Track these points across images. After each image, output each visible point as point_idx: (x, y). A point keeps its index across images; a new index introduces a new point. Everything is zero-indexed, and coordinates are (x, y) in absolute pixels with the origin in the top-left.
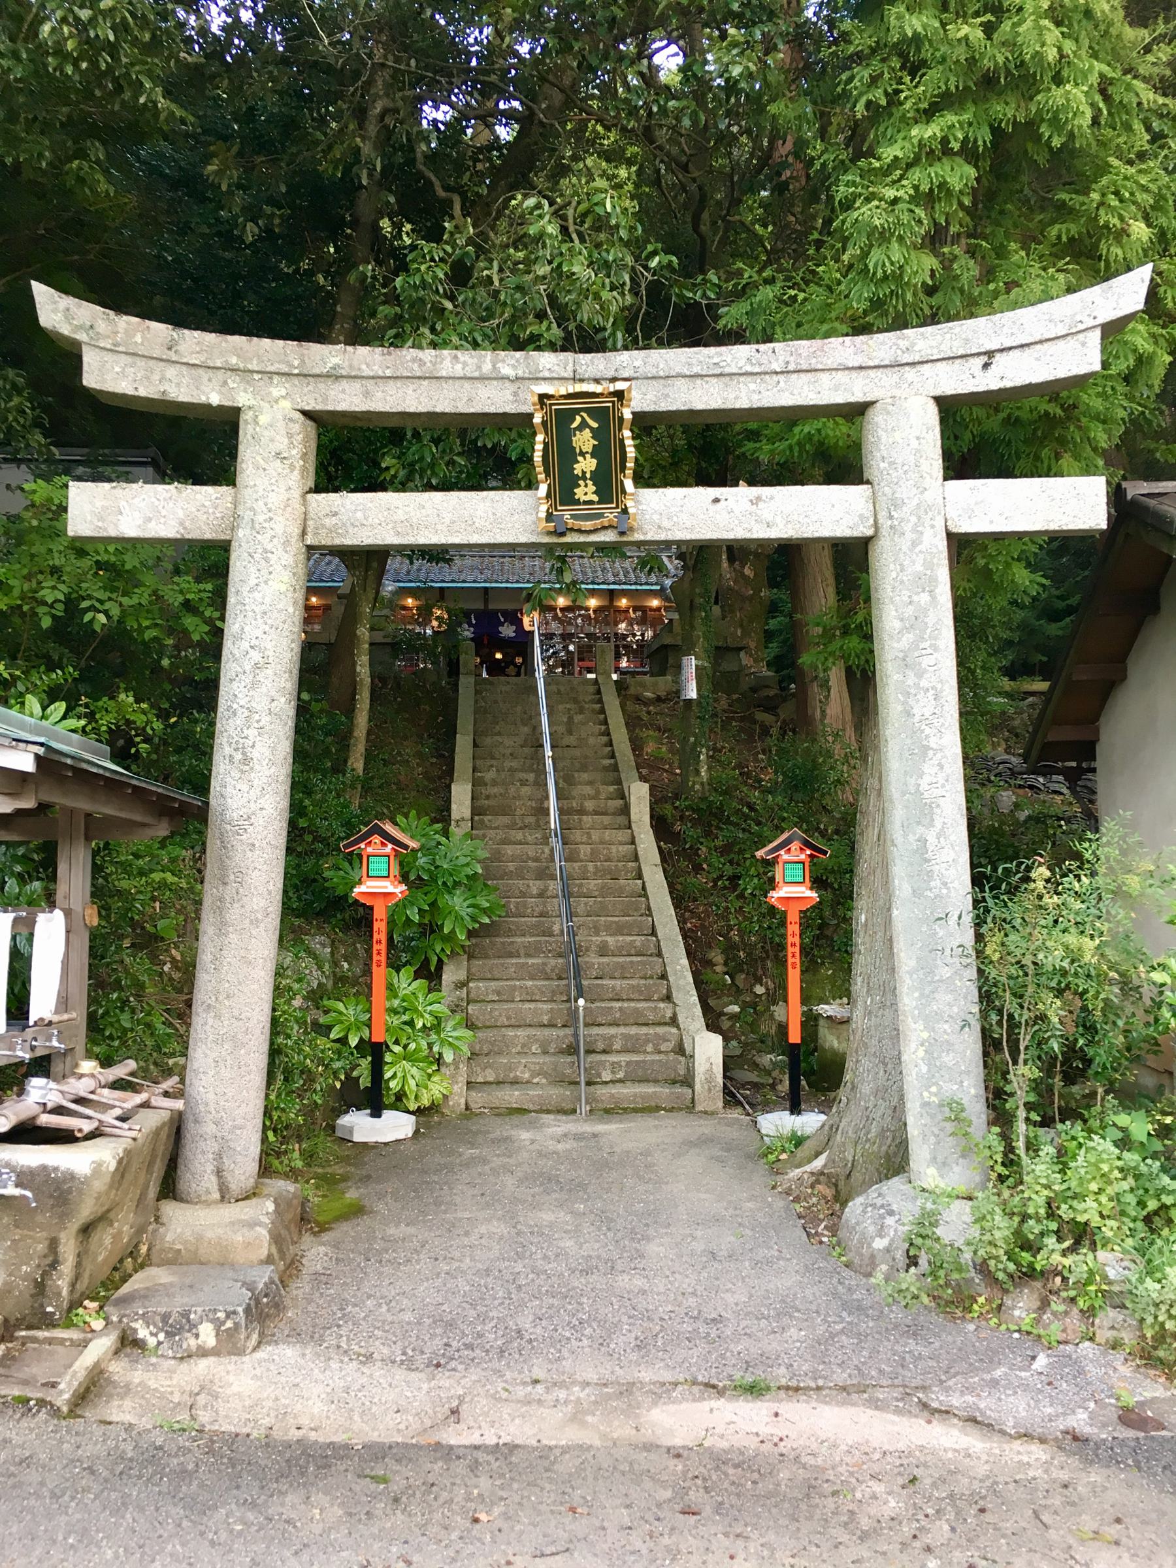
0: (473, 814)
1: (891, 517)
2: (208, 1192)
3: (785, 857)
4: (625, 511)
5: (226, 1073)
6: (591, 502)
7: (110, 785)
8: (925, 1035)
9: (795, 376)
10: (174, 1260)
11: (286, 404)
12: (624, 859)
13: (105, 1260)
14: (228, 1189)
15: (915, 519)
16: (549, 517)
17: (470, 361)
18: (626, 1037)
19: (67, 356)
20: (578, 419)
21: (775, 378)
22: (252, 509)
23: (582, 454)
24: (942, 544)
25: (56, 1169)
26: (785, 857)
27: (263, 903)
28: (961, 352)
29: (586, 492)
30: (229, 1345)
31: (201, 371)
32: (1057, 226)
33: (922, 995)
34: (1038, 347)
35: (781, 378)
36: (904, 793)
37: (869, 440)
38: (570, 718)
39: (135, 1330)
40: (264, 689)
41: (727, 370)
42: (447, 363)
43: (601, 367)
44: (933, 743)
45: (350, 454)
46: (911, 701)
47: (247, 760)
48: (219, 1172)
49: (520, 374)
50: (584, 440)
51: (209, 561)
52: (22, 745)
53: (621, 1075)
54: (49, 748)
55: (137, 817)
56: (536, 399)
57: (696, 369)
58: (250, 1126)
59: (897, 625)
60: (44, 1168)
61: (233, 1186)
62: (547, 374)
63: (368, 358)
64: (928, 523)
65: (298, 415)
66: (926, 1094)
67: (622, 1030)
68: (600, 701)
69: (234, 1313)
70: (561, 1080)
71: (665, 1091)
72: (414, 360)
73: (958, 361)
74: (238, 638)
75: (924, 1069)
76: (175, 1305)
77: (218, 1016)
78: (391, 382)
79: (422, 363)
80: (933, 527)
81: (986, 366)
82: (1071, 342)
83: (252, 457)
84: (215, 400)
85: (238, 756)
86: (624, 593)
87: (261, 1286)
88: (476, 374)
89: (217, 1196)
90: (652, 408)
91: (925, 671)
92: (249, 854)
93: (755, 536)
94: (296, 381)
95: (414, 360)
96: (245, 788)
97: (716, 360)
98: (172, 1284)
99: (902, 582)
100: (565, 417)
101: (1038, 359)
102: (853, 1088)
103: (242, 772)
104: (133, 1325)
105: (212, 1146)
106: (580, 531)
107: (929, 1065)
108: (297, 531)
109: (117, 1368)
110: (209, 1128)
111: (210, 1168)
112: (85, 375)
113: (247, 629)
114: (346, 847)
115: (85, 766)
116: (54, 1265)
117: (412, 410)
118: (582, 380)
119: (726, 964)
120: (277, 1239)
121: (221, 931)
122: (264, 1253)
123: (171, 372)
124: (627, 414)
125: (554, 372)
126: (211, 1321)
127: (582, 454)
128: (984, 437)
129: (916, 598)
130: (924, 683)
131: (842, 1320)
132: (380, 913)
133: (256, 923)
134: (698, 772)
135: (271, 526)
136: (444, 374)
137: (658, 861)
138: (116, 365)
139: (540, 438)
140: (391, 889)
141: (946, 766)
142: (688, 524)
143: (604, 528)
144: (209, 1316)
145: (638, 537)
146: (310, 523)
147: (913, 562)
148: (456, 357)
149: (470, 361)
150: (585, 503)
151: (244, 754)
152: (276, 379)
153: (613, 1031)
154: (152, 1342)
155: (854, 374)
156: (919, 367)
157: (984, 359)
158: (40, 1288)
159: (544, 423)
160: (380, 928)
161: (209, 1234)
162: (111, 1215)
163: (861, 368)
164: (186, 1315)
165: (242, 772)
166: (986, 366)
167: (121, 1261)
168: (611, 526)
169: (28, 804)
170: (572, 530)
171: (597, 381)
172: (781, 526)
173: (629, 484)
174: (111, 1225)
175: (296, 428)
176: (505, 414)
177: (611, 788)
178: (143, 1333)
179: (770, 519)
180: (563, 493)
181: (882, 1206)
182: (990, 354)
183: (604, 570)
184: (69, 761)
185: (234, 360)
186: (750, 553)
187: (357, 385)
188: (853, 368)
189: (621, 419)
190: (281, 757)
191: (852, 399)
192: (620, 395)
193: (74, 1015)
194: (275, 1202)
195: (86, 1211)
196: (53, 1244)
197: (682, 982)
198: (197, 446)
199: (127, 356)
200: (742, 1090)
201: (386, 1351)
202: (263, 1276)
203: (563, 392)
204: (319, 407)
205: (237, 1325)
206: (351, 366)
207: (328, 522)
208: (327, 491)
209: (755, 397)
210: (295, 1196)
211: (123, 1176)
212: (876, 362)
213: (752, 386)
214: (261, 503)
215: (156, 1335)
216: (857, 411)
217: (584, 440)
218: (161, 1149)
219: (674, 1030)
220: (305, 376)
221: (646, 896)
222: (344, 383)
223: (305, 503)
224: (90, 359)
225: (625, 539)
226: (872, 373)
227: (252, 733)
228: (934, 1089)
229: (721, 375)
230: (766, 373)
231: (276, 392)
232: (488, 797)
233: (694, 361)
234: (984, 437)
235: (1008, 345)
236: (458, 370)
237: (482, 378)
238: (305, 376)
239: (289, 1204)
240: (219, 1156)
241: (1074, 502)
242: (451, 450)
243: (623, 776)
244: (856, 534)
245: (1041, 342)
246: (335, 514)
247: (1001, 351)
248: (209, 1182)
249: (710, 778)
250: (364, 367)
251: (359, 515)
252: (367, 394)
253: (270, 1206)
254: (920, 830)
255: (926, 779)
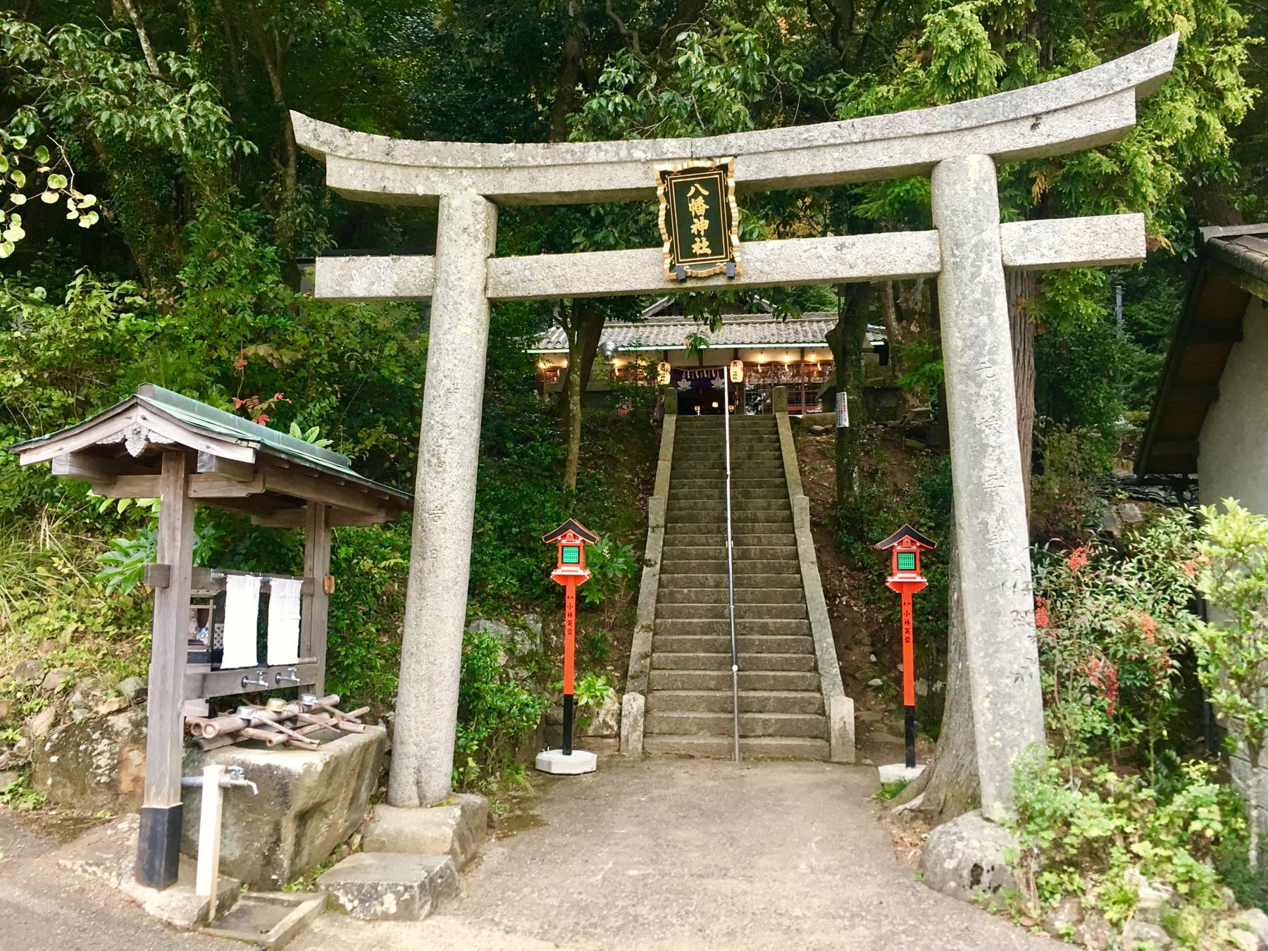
0: (666, 522)
1: (954, 256)
2: (410, 798)
3: (899, 548)
4: (733, 260)
5: (424, 706)
6: (706, 255)
7: (350, 485)
8: (990, 688)
9: (870, 145)
10: (381, 847)
11: (473, 192)
12: (787, 557)
13: (322, 844)
14: (425, 797)
15: (978, 253)
16: (672, 267)
17: (610, 149)
18: (779, 700)
19: (312, 165)
20: (693, 189)
21: (855, 147)
22: (446, 272)
23: (697, 217)
24: (1000, 277)
25: (277, 768)
26: (899, 548)
27: (452, 574)
28: (1012, 116)
29: (702, 246)
30: (406, 913)
31: (410, 170)
32: (1113, 14)
33: (987, 655)
34: (1080, 108)
35: (860, 147)
36: (968, 484)
37: (936, 192)
38: (751, 447)
39: (338, 897)
40: (454, 409)
41: (815, 143)
42: (593, 152)
43: (713, 147)
44: (992, 441)
45: (528, 225)
46: (973, 407)
47: (441, 463)
48: (418, 783)
49: (649, 157)
50: (698, 206)
51: (416, 313)
52: (245, 443)
53: (771, 731)
54: (264, 445)
55: (359, 508)
56: (658, 176)
57: (789, 145)
58: (442, 748)
59: (960, 343)
60: (269, 767)
61: (429, 795)
62: (670, 156)
63: (533, 152)
64: (985, 258)
65: (483, 200)
66: (991, 739)
67: (775, 694)
68: (777, 433)
69: (411, 887)
70: (722, 730)
71: (807, 742)
72: (567, 151)
73: (1009, 124)
74: (436, 370)
75: (990, 717)
76: (367, 879)
77: (418, 662)
78: (551, 169)
79: (573, 152)
80: (989, 261)
81: (1034, 126)
82: (1109, 102)
83: (446, 232)
84: (421, 190)
85: (434, 461)
86: (813, 350)
87: (437, 869)
88: (615, 159)
89: (417, 802)
90: (754, 178)
91: (984, 382)
92: (442, 536)
93: (840, 276)
94: (480, 173)
95: (567, 151)
96: (439, 484)
97: (805, 136)
98: (371, 866)
99: (964, 308)
100: (682, 189)
101: (1080, 118)
102: (947, 738)
103: (437, 472)
104: (336, 893)
105: (413, 763)
106: (697, 278)
107: (993, 714)
108: (481, 287)
109: (318, 925)
110: (411, 749)
111: (412, 779)
112: (328, 178)
113: (442, 363)
114: (547, 539)
115: (298, 461)
116: (277, 842)
117: (567, 190)
118: (698, 159)
119: (873, 645)
120: (461, 837)
121: (421, 597)
122: (447, 847)
123: (389, 172)
124: (731, 183)
125: (680, 151)
126: (394, 893)
127: (697, 217)
128: (1041, 184)
129: (975, 321)
130: (983, 392)
131: (905, 922)
132: (571, 592)
133: (447, 589)
134: (851, 488)
135: (463, 280)
136: (590, 160)
137: (815, 559)
138: (351, 168)
139: (663, 206)
140: (581, 573)
141: (1004, 460)
142: (785, 269)
143: (716, 274)
144: (392, 888)
145: (744, 280)
146: (491, 280)
147: (973, 291)
148: (599, 147)
149: (610, 149)
150: (701, 255)
151: (439, 458)
152: (465, 172)
153: (766, 694)
154: (349, 906)
155: (921, 140)
156: (976, 131)
157: (1032, 121)
158: (269, 861)
159: (666, 194)
160: (571, 602)
161: (407, 830)
162: (326, 808)
163: (927, 134)
164: (375, 887)
165: (437, 472)
166: (1034, 126)
167: (338, 846)
168: (722, 273)
169: (258, 489)
170: (691, 277)
171: (710, 158)
172: (861, 267)
173: (735, 239)
174: (326, 817)
175: (480, 208)
176: (638, 189)
177: (781, 501)
178: (343, 900)
179: (852, 261)
180: (684, 248)
181: (955, 833)
182: (1037, 116)
183: (796, 332)
184: (283, 456)
185: (434, 160)
186: (916, 313)
187: (525, 173)
188: (920, 135)
189: (727, 187)
190: (467, 460)
191: (919, 161)
192: (724, 168)
193: (315, 659)
194: (463, 809)
195: (300, 802)
196: (277, 828)
197: (827, 657)
198: (406, 226)
199: (358, 162)
200: (867, 744)
201: (528, 925)
202: (440, 862)
203: (680, 169)
204: (496, 192)
205: (412, 897)
206: (520, 159)
207: (504, 279)
208: (503, 256)
209: (838, 164)
210: (481, 807)
211: (331, 777)
212: (940, 129)
213: (836, 155)
214: (453, 266)
215: (351, 901)
216: (927, 170)
217: (698, 206)
218: (370, 762)
219: (817, 695)
220: (487, 168)
221: (803, 588)
222: (515, 173)
223: (487, 266)
224: (332, 166)
225: (734, 282)
226: (936, 139)
227: (444, 442)
228: (998, 735)
229: (809, 147)
230: (846, 144)
231: (465, 182)
232: (681, 509)
233: (788, 138)
234: (1041, 184)
235: (1053, 107)
236: (602, 157)
237: (620, 162)
238: (487, 168)
239: (475, 812)
240: (419, 771)
241: (1120, 236)
242: (628, 230)
243: (790, 492)
244: (925, 270)
245: (1082, 104)
246: (509, 273)
247: (1047, 113)
248: (412, 791)
249: (861, 493)
250: (530, 159)
251: (527, 272)
252: (533, 180)
253: (457, 812)
254: (982, 515)
255: (989, 471)
